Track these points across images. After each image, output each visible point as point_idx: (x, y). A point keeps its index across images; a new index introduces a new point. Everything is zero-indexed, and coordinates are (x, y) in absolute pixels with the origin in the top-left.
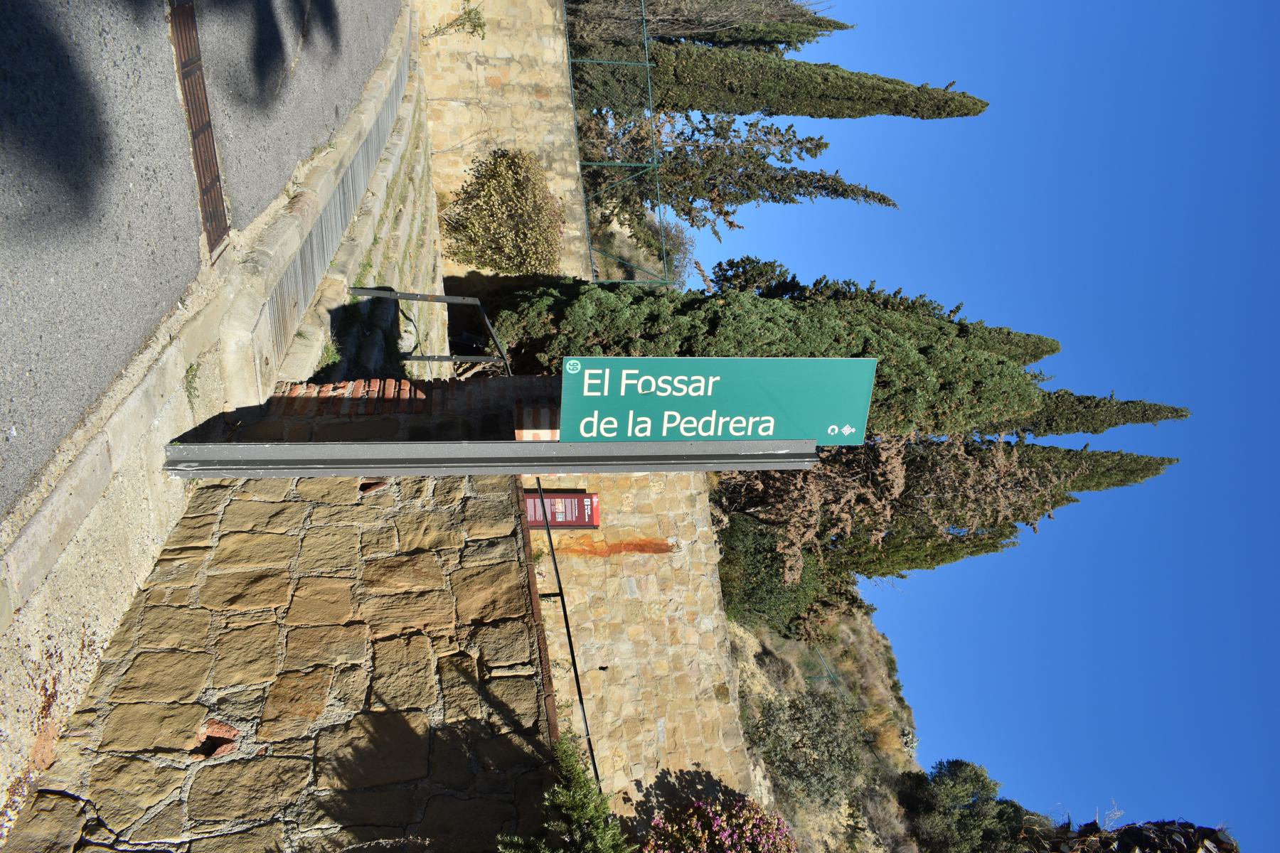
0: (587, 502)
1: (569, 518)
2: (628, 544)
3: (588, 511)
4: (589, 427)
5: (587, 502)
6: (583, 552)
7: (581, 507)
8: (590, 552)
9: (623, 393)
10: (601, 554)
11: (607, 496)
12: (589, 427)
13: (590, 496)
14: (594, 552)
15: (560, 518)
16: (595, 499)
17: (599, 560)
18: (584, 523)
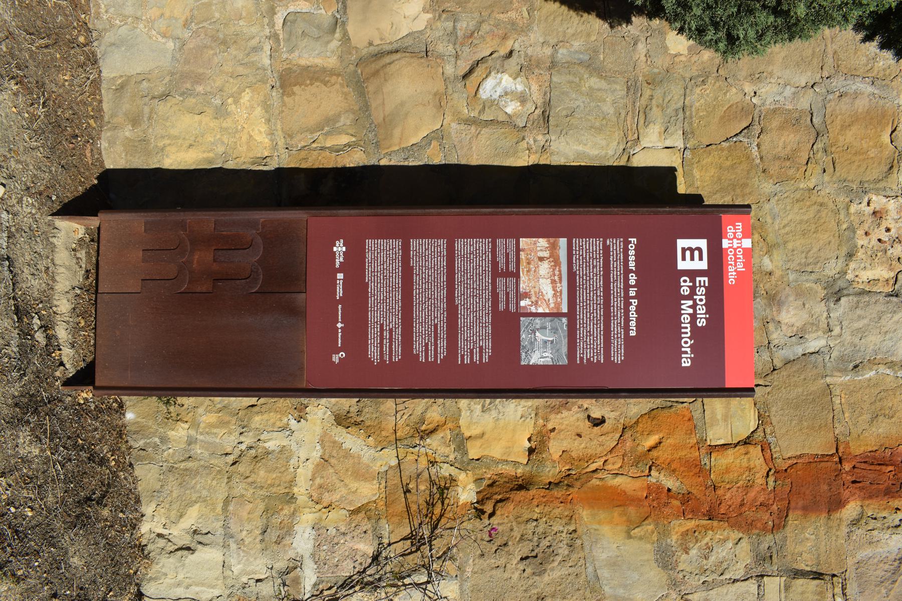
0: (691, 254)
1: (590, 350)
2: (875, 460)
3: (692, 311)
4: (685, 281)
5: (691, 254)
6: (655, 505)
7: (659, 281)
8: (688, 504)
9: (686, 363)
10: (738, 518)
11: (777, 209)
12: (685, 281)
13: (702, 215)
14: (706, 506)
15: (541, 349)
16: (735, 240)
17: (732, 549)
18: (662, 363)
